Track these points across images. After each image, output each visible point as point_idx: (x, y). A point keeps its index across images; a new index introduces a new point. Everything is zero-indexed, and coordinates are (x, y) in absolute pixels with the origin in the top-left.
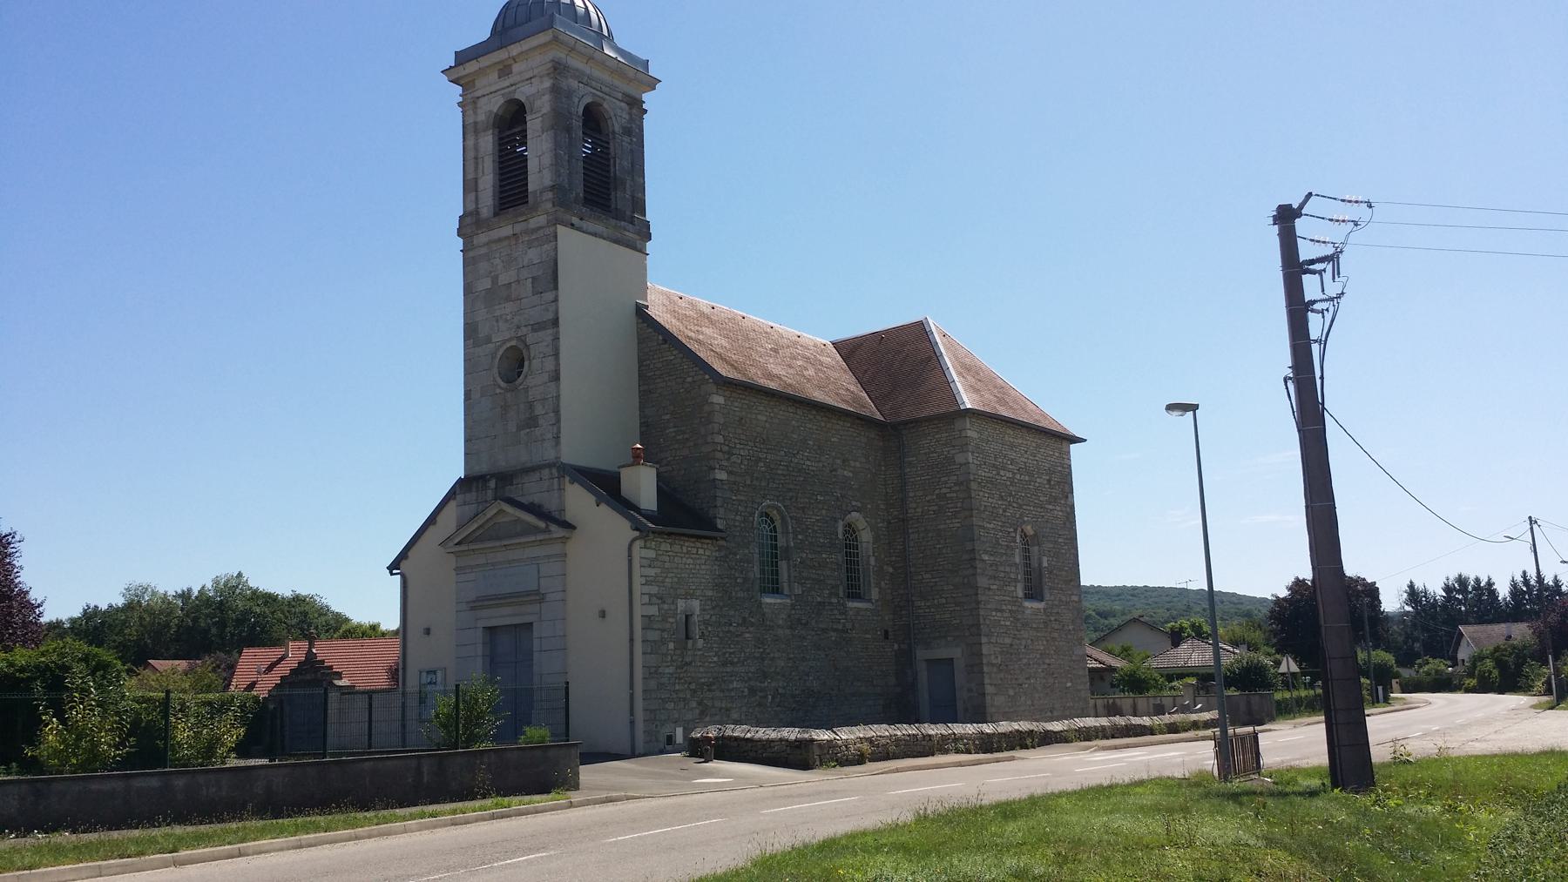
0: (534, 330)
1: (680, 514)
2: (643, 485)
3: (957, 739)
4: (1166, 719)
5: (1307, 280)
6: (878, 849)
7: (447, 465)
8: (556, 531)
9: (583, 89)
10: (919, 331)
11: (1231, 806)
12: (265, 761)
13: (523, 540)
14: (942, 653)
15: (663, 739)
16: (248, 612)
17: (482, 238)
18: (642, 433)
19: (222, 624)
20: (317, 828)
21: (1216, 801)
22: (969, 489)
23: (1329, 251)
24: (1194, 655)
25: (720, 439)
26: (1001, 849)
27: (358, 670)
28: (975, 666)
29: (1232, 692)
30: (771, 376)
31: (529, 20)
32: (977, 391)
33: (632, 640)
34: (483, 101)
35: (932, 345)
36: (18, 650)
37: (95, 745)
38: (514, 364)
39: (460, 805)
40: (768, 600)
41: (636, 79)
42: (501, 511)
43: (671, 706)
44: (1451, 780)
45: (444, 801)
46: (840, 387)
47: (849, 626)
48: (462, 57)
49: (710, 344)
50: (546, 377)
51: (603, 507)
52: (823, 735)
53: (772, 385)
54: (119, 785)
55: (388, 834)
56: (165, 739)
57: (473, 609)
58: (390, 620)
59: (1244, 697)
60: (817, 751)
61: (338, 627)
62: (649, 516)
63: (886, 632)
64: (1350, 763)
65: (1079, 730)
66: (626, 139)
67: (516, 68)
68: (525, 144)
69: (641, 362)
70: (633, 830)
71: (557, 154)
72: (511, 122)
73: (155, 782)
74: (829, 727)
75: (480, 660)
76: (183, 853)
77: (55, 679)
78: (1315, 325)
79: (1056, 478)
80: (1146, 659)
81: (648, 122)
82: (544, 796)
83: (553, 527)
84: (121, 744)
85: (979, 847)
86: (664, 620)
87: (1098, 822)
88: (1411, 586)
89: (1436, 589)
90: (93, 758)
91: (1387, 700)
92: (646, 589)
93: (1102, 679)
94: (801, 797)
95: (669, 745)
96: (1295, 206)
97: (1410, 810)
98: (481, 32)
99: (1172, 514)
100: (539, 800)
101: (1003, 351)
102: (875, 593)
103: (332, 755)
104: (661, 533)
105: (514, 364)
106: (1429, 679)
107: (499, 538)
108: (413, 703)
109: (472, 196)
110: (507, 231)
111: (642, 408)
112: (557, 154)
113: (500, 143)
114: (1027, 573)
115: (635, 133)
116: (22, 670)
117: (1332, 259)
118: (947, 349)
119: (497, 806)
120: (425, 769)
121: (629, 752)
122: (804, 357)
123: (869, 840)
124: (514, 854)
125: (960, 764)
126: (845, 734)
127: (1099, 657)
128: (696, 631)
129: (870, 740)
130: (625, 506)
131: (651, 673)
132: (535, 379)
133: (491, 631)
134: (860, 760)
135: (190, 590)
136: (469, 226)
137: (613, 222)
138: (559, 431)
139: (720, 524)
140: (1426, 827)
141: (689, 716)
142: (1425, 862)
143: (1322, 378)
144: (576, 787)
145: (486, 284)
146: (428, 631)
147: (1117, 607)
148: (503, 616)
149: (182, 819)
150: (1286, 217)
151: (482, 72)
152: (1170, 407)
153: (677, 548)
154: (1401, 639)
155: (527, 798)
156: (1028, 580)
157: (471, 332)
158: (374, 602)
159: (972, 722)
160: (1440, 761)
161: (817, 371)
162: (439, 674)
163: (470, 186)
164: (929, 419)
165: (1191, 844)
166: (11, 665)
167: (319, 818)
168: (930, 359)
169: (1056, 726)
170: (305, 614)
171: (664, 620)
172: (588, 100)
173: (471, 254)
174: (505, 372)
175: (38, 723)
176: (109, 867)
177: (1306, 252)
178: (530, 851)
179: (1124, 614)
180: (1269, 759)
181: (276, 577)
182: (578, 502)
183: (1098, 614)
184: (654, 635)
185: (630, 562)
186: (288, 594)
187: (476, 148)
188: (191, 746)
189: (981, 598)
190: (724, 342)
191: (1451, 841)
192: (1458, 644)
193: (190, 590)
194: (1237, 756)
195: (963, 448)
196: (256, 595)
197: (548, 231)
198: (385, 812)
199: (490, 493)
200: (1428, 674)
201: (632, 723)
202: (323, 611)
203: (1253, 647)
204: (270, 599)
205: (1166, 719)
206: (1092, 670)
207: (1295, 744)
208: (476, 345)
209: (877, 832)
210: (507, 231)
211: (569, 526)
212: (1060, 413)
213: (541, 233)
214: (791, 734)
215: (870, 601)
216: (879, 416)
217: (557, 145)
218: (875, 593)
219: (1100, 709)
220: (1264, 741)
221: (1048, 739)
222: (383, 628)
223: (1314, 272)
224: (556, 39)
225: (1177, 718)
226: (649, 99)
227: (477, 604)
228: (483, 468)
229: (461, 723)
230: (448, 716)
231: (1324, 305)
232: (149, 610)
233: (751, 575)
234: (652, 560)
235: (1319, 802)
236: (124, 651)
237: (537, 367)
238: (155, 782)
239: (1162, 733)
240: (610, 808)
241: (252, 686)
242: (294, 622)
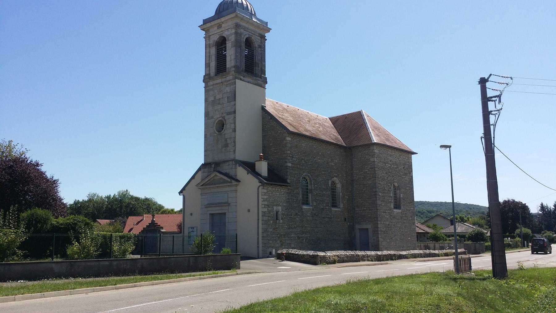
0: (227, 115)
1: (275, 178)
2: (263, 167)
3: (368, 256)
4: (444, 251)
6: (331, 292)
7: (198, 159)
8: (234, 183)
9: (245, 33)
10: (359, 115)
11: (453, 282)
12: (139, 256)
14: (364, 226)
15: (268, 253)
16: (129, 204)
17: (211, 83)
18: (263, 150)
19: (121, 208)
20: (158, 279)
21: (448, 281)
22: (375, 170)
23: (498, 93)
24: (460, 228)
25: (289, 152)
26: (370, 294)
27: (168, 225)
28: (376, 231)
29: (470, 242)
30: (307, 130)
31: (228, 9)
32: (378, 136)
33: (258, 220)
34: (212, 37)
35: (363, 120)
36: (60, 218)
37: (89, 251)
38: (221, 126)
39: (202, 273)
40: (305, 207)
41: (264, 28)
42: (216, 175)
43: (271, 242)
45: (197, 271)
46: (331, 134)
48: (205, 22)
49: (286, 119)
50: (231, 130)
52: (322, 254)
53: (307, 134)
54: (97, 263)
56: (111, 249)
57: (206, 207)
60: (319, 259)
61: (160, 209)
62: (265, 178)
63: (345, 219)
64: (500, 269)
65: (412, 254)
66: (260, 49)
67: (223, 25)
68: (225, 51)
70: (257, 283)
71: (236, 54)
72: (221, 44)
73: (107, 263)
75: (208, 224)
76: (118, 286)
77: (72, 227)
78: (492, 119)
79: (406, 166)
80: (440, 228)
83: (233, 181)
84: (97, 251)
85: (363, 293)
86: (269, 213)
87: (405, 286)
88: (542, 204)
90: (88, 255)
92: (264, 203)
93: (424, 236)
95: (270, 255)
96: (486, 78)
97: (517, 286)
98: (211, 13)
100: (227, 272)
101: (388, 123)
105: (221, 126)
107: (215, 184)
110: (219, 81)
111: (263, 141)
112: (236, 54)
113: (218, 50)
114: (395, 199)
115: (262, 47)
116: (61, 224)
117: (499, 97)
118: (369, 121)
119: (214, 273)
120: (191, 261)
123: (329, 289)
124: (219, 289)
125: (368, 265)
126: (329, 254)
127: (421, 228)
128: (280, 217)
129: (338, 256)
130: (257, 174)
131: (265, 231)
132: (227, 131)
133: (212, 215)
134: (334, 262)
135: (110, 195)
136: (207, 79)
137: (255, 78)
139: (289, 181)
141: (277, 246)
143: (494, 137)
144: (239, 268)
145: (212, 99)
146: (191, 214)
147: (435, 209)
148: (216, 210)
149: (117, 275)
150: (483, 82)
151: (212, 27)
152: (442, 146)
153: (274, 189)
154: (537, 223)
155: (223, 271)
156: (395, 202)
157: (207, 115)
158: (174, 203)
159: (374, 251)
162: (195, 229)
163: (207, 65)
164: (361, 146)
165: (431, 294)
166: (58, 223)
167: (159, 276)
168: (362, 125)
169: (404, 253)
170: (149, 204)
172: (247, 36)
173: (207, 88)
174: (218, 128)
176: (97, 289)
177: (490, 94)
178: (224, 288)
180: (474, 267)
181: (139, 191)
182: (241, 173)
183: (428, 212)
186: (143, 197)
187: (210, 53)
189: (378, 208)
190: (291, 119)
191: (528, 297)
193: (110, 195)
194: (462, 266)
195: (373, 156)
196: (132, 197)
197: (232, 81)
201: (258, 247)
202: (155, 204)
203: (481, 226)
204: (137, 199)
205: (444, 251)
207: (482, 262)
208: (208, 119)
209: (333, 287)
211: (239, 181)
212: (408, 144)
213: (230, 82)
214: (311, 253)
215: (340, 208)
217: (236, 52)
219: (422, 247)
220: (473, 260)
221: (401, 257)
223: (492, 101)
224: (237, 16)
228: (210, 160)
229: (202, 246)
230: (198, 244)
232: (96, 202)
234: (265, 193)
235: (485, 282)
238: (107, 263)
239: (442, 256)
240: (250, 275)
242: (145, 207)
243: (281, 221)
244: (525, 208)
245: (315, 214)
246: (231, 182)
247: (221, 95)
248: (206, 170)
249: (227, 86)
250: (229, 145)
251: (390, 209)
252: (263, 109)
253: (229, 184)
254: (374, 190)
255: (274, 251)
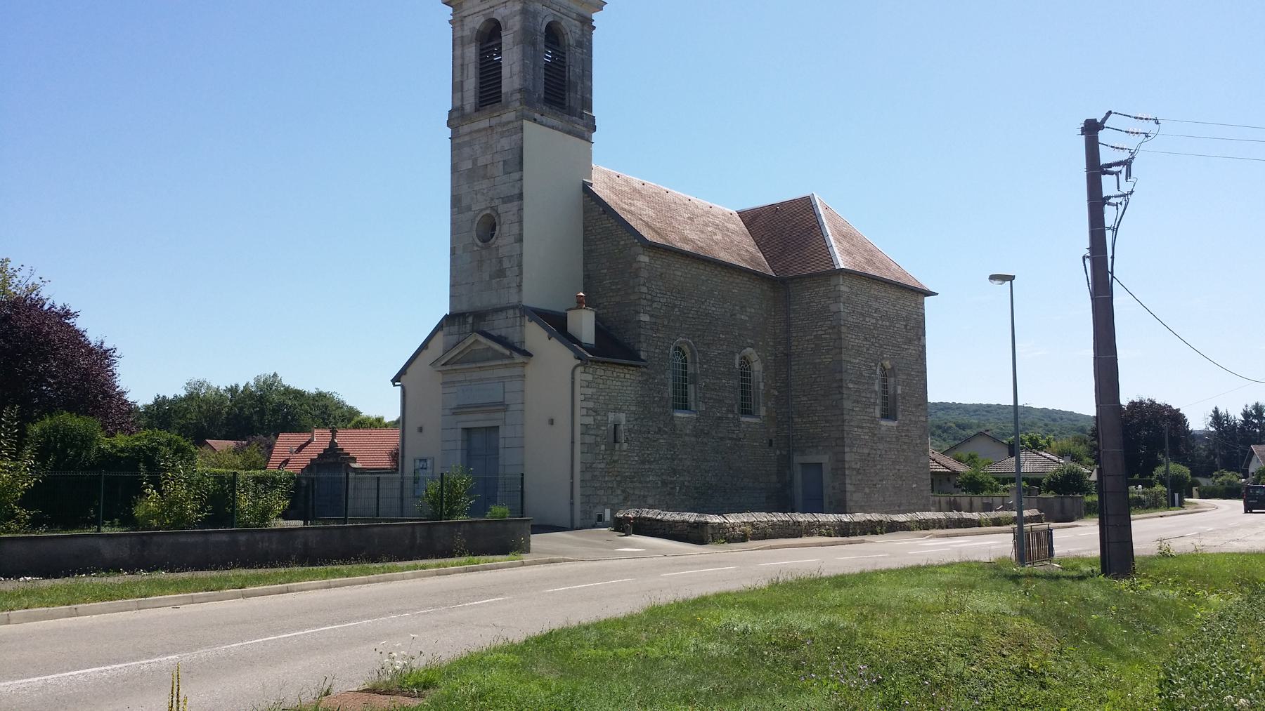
0: (504, 202)
1: (612, 347)
2: (584, 324)
3: (821, 525)
4: (993, 514)
5: (1106, 179)
7: (433, 303)
8: (519, 358)
9: (546, 11)
11: (1012, 585)
12: (299, 524)
13: (493, 363)
14: (812, 458)
15: (595, 517)
17: (465, 129)
19: (262, 414)
20: (341, 575)
22: (840, 332)
23: (1125, 156)
24: (1030, 464)
25: (644, 289)
26: (821, 609)
27: (367, 453)
28: (839, 469)
30: (686, 240)
33: (573, 442)
34: (468, 20)
36: (119, 435)
37: (183, 509)
38: (489, 229)
39: (442, 561)
40: (679, 414)
44: (1196, 572)
46: (741, 249)
47: (741, 436)
49: (639, 215)
50: (512, 239)
51: (554, 341)
53: (687, 248)
54: (200, 539)
55: (391, 580)
56: (233, 507)
58: (391, 412)
59: (1063, 498)
60: (710, 531)
61: (350, 418)
62: (588, 349)
64: (1117, 555)
65: (920, 522)
69: (585, 228)
70: (566, 584)
71: (526, 68)
72: (490, 36)
73: (225, 538)
74: (719, 513)
75: (459, 453)
76: (249, 589)
77: (147, 457)
78: (1110, 215)
80: (987, 465)
81: (596, 36)
82: (504, 557)
83: (516, 355)
84: (202, 510)
86: (598, 427)
87: (901, 592)
88: (1216, 411)
89: (1237, 415)
91: (1181, 505)
92: (585, 404)
94: (694, 564)
95: (599, 522)
97: (1156, 593)
99: (1000, 352)
101: (871, 224)
102: (763, 411)
103: (352, 521)
104: (597, 362)
105: (489, 229)
106: (1221, 488)
107: (474, 362)
108: (409, 484)
109: (459, 94)
110: (484, 123)
111: (585, 264)
112: (526, 68)
114: (884, 398)
115: (585, 45)
116: (122, 450)
117: (1127, 163)
118: (828, 220)
119: (469, 562)
121: (569, 526)
122: (714, 224)
124: (480, 597)
125: (821, 545)
126: (732, 519)
127: (942, 463)
129: (752, 524)
130: (570, 340)
131: (587, 467)
132: (503, 240)
134: (743, 538)
135: (237, 386)
136: (456, 118)
137: (566, 117)
138: (521, 281)
139: (643, 355)
140: (1165, 609)
141: (615, 501)
142: (1156, 632)
143: (1113, 257)
144: (528, 551)
145: (468, 165)
146: (421, 430)
147: (974, 421)
150: (1091, 129)
152: (993, 278)
153: (609, 373)
154: (1204, 454)
155: (491, 558)
156: (885, 404)
157: (456, 201)
158: (382, 403)
159: (833, 513)
160: (1196, 556)
161: (724, 235)
163: (457, 87)
164: (811, 276)
165: (962, 610)
166: (114, 446)
169: (901, 518)
171: (598, 427)
173: (457, 141)
174: (482, 232)
175: (143, 494)
176: (199, 597)
177: (1106, 157)
178: (491, 596)
179: (979, 426)
180: (1058, 550)
181: (303, 377)
182: (535, 336)
183: (958, 426)
184: (589, 439)
185: (573, 383)
188: (250, 513)
189: (846, 417)
190: (651, 213)
191: (1180, 618)
192: (1250, 460)
193: (237, 386)
194: (1032, 547)
195: (836, 300)
196: (288, 391)
197: (516, 124)
198: (389, 564)
199: (468, 327)
200: (1222, 484)
202: (340, 405)
203: (1076, 458)
204: (299, 395)
205: (993, 514)
206: (934, 473)
207: (1079, 539)
209: (739, 593)
210: (484, 123)
211: (528, 354)
213: (511, 126)
214: (692, 517)
215: (758, 416)
216: (771, 273)
218: (763, 411)
220: (1056, 535)
221: (893, 527)
222: (386, 420)
223: (1112, 173)
225: (1001, 514)
226: (597, 17)
227: (458, 410)
228: (464, 307)
229: (444, 502)
230: (435, 496)
231: (1118, 200)
232: (205, 400)
233: (666, 395)
234: (589, 382)
236: (184, 431)
237: (505, 232)
238: (225, 538)
240: (552, 567)
241: (286, 462)
243: (625, 446)
244: (1176, 418)
245: (702, 430)
246: (511, 357)
247: (489, 157)
248: (455, 329)
249: (502, 135)
250: (508, 273)
251: (873, 420)
252: (586, 189)
253: (506, 362)
254: (838, 377)
255: (607, 513)
